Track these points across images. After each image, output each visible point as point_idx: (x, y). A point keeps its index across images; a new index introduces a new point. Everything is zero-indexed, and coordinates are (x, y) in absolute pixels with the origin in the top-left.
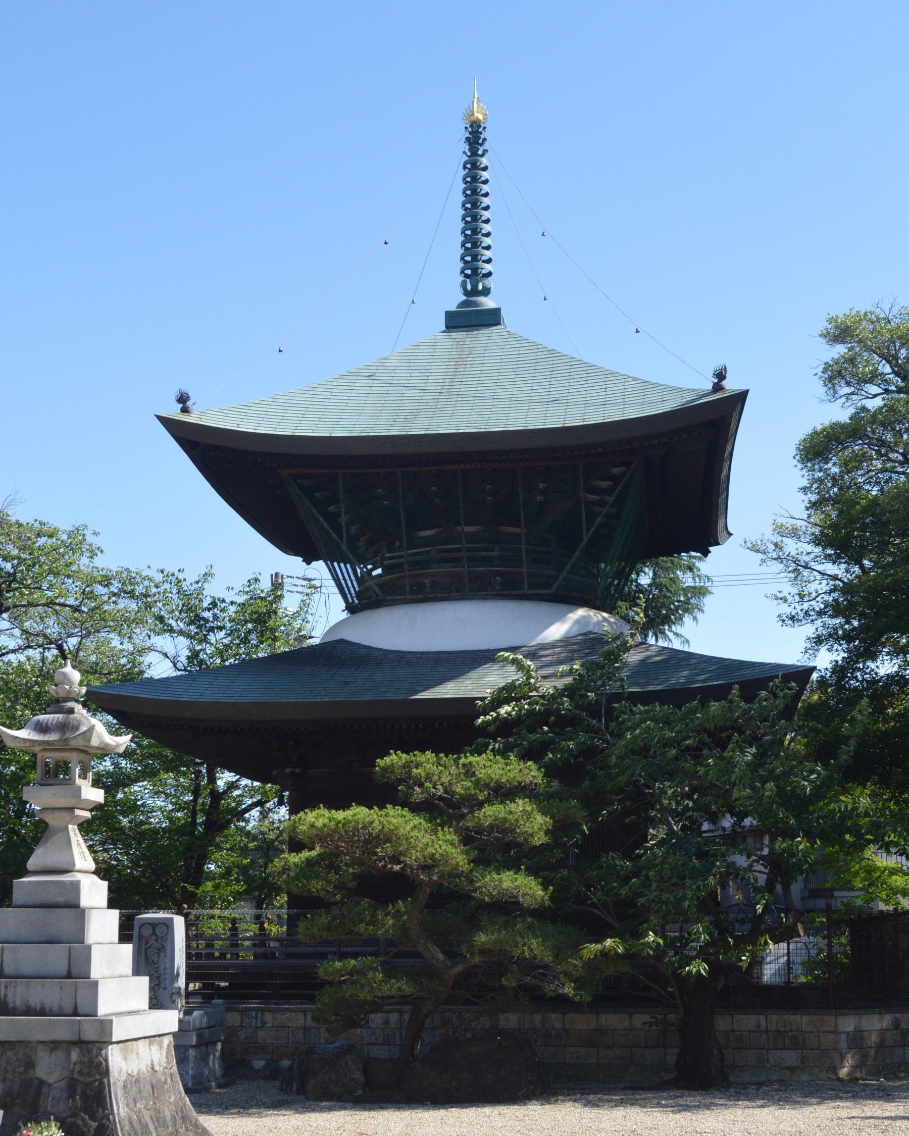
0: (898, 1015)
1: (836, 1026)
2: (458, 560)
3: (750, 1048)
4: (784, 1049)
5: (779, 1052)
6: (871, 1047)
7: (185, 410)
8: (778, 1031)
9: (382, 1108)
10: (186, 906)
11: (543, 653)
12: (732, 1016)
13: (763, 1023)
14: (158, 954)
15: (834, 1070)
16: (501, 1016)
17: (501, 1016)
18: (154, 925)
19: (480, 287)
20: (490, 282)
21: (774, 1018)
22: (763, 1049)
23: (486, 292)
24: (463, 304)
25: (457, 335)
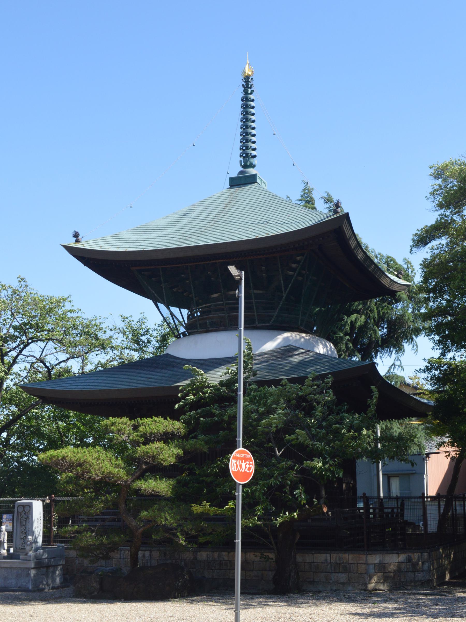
0: (411, 555)
1: (367, 560)
2: (223, 310)
3: (322, 572)
4: (339, 572)
5: (336, 574)
6: (391, 572)
7: (77, 241)
8: (336, 563)
9: (140, 602)
10: (53, 496)
11: (257, 358)
12: (313, 554)
13: (329, 558)
14: (26, 521)
15: (366, 584)
16: (199, 554)
17: (199, 554)
18: (24, 506)
19: (249, 164)
20: (255, 161)
21: (334, 556)
22: (329, 572)
23: (253, 166)
24: (241, 172)
25: (233, 190)
